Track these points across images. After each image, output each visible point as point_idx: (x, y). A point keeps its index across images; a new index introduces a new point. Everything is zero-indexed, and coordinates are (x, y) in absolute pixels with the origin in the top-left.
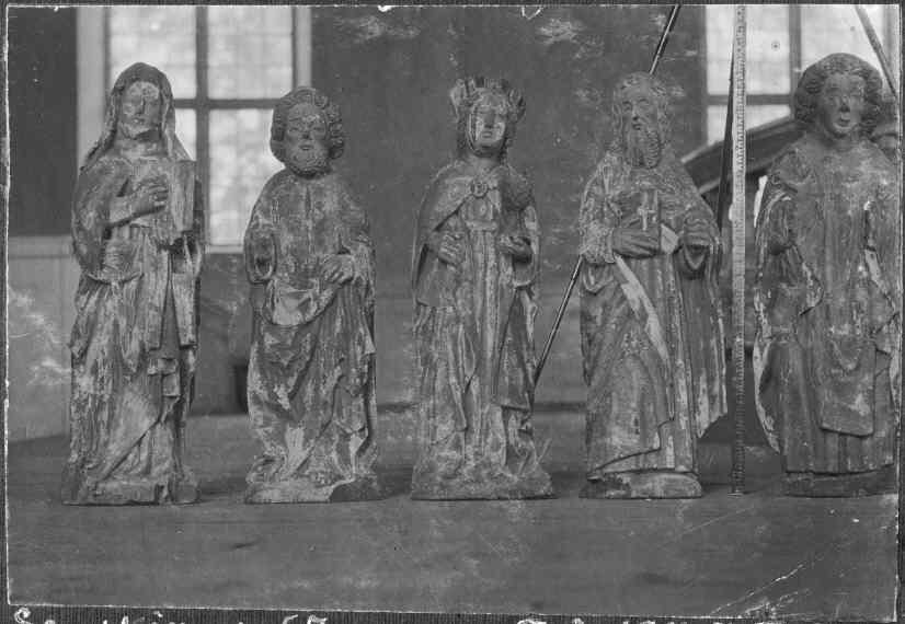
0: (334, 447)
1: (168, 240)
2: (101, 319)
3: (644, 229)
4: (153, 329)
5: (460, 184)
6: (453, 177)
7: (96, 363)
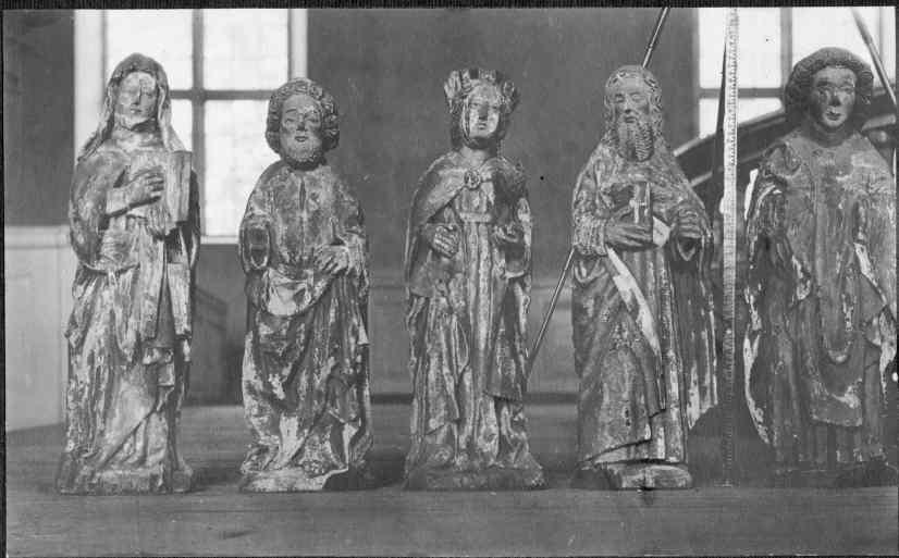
1: (164, 230)
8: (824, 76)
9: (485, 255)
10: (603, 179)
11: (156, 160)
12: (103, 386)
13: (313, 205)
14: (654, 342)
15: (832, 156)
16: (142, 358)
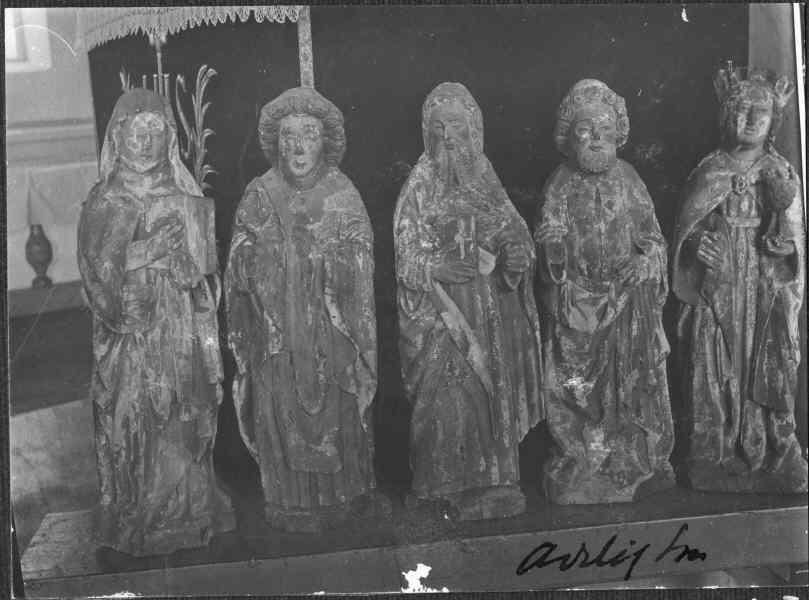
0: (634, 444)
1: (191, 284)
2: (127, 371)
3: (462, 257)
4: (185, 380)
5: (722, 179)
6: (715, 170)
7: (128, 419)
8: (287, 125)
9: (753, 263)
10: (425, 207)
11: (172, 205)
12: (142, 450)
13: (611, 216)
14: (485, 378)
15: (303, 201)
16: (178, 415)
